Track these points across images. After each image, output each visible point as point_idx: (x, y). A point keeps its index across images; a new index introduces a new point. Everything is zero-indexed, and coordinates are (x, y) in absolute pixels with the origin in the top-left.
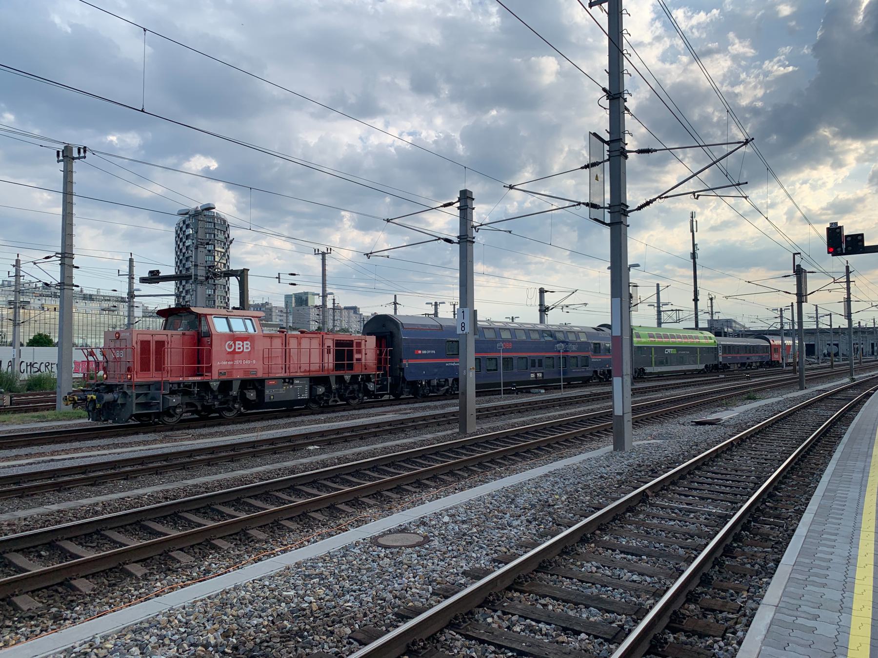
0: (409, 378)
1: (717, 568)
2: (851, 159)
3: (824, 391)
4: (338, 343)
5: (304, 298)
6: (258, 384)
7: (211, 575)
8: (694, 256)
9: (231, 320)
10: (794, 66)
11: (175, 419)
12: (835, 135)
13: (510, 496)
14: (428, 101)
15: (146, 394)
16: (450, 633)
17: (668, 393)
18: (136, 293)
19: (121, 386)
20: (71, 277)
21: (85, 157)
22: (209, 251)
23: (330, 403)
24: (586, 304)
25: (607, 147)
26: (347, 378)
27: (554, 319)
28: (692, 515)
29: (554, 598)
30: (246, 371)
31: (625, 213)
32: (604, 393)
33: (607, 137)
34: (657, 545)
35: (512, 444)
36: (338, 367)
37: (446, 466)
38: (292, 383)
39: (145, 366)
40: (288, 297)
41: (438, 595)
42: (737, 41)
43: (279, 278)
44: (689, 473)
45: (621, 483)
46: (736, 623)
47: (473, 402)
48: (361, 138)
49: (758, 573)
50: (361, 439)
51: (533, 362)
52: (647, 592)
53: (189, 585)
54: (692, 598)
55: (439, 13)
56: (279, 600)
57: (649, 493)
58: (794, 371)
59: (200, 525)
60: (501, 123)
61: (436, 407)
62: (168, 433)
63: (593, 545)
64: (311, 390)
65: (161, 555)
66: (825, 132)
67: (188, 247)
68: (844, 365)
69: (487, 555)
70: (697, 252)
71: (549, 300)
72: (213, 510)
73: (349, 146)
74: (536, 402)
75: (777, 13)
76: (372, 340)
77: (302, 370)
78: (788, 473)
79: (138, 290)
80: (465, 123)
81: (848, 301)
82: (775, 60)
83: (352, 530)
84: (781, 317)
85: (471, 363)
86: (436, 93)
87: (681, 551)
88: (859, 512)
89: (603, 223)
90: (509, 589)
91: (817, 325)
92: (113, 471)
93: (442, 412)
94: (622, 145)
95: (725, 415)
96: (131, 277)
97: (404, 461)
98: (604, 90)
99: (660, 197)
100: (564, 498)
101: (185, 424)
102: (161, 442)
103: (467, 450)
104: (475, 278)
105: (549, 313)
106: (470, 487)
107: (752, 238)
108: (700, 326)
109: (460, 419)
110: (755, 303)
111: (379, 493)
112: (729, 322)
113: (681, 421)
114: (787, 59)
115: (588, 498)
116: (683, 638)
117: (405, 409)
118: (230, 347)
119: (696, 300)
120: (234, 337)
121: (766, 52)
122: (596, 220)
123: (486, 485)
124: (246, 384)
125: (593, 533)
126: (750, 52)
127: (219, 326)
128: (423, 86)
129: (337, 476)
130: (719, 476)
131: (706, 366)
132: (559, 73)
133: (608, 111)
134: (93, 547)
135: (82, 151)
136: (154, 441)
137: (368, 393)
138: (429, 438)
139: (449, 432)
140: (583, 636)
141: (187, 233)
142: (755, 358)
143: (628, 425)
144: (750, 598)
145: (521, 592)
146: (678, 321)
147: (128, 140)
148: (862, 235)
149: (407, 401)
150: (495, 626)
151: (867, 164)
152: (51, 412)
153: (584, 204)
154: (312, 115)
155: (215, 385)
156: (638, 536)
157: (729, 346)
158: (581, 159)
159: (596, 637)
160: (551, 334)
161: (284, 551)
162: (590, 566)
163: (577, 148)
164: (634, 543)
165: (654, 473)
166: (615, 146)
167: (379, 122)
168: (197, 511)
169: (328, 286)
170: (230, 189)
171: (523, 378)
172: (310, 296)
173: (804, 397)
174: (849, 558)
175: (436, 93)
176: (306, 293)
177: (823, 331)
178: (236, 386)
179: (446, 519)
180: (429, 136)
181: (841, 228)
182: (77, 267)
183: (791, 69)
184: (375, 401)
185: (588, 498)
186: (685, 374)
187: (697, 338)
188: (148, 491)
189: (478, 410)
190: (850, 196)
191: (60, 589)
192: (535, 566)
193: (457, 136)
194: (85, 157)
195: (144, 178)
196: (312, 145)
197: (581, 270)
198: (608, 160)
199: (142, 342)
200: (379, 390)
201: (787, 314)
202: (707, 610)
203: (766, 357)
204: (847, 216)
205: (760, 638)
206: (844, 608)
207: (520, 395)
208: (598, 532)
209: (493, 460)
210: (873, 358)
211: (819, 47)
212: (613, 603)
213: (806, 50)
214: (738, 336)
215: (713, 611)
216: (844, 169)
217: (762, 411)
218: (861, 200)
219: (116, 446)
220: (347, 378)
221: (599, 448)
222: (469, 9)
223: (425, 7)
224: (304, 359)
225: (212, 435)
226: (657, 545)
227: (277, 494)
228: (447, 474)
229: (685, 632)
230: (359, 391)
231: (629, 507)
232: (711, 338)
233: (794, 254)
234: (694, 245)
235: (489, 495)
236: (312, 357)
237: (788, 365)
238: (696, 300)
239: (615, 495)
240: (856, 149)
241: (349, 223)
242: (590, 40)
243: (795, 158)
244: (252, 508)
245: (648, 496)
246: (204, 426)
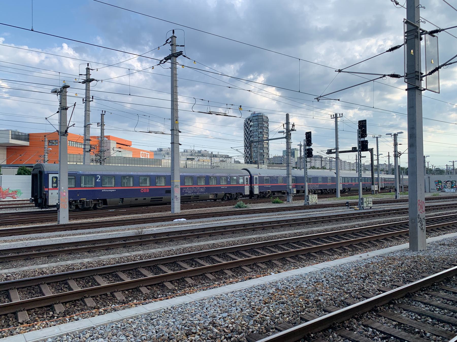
35: (384, 233)
103: (370, 232)
153: (388, 75)
168: (233, 253)
188: (304, 231)
209: (331, 249)
239: (446, 267)
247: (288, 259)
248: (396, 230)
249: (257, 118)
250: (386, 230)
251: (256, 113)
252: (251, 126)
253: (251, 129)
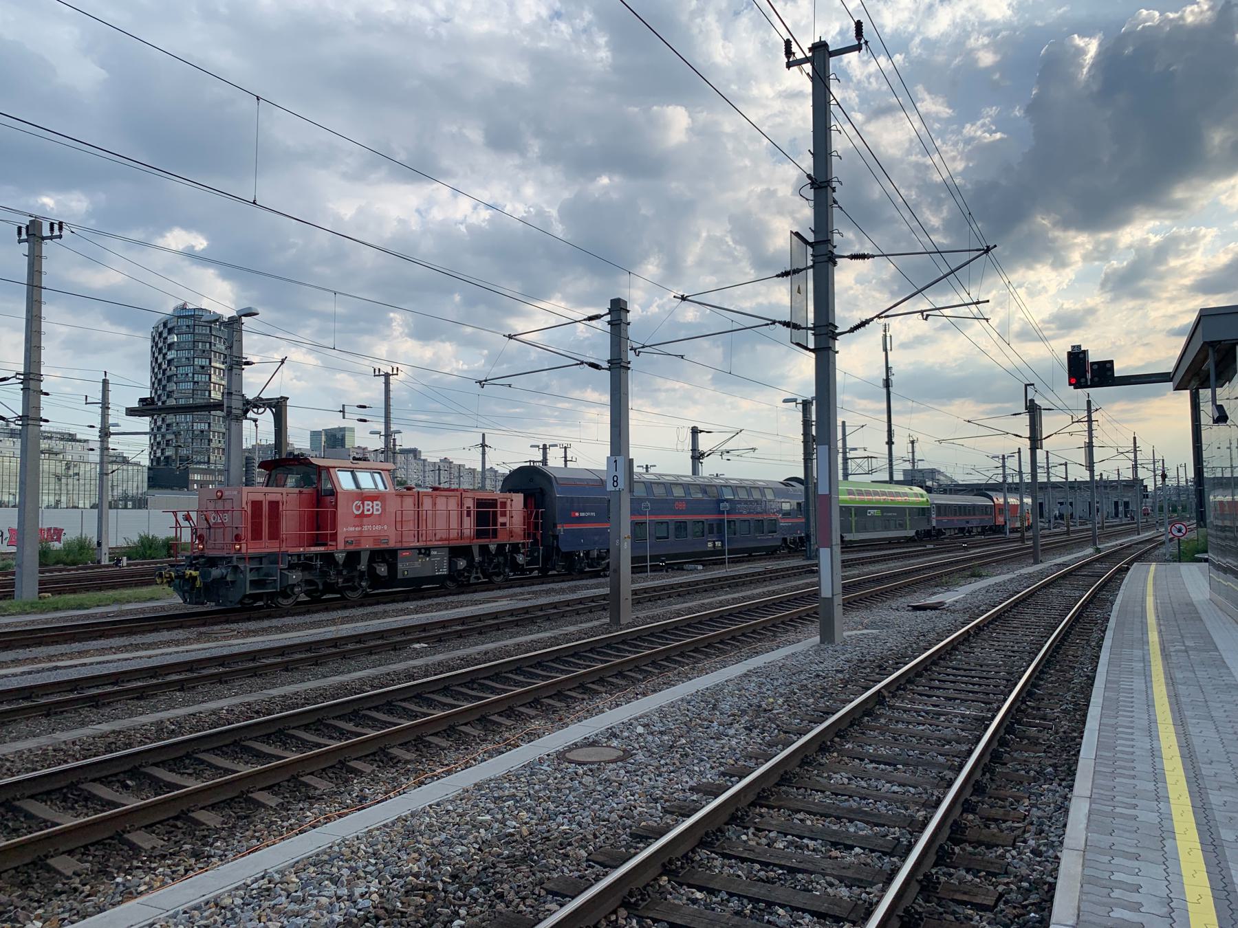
0: (564, 549)
1: (988, 775)
2: (1076, 256)
3: (1065, 565)
4: (480, 503)
5: (339, 436)
6: (388, 556)
7: (369, 802)
8: (887, 384)
9: (358, 474)
10: (1003, 132)
11: (291, 601)
12: (1055, 225)
13: (712, 699)
14: (512, 161)
15: (258, 569)
16: (704, 853)
17: (866, 569)
18: (112, 430)
19: (228, 559)
20: (38, 408)
21: (60, 237)
22: (203, 367)
23: (472, 581)
24: (754, 449)
25: (810, 250)
26: (493, 547)
27: (709, 468)
28: (942, 719)
29: (809, 813)
30: (377, 540)
31: (834, 336)
32: (782, 570)
33: (811, 238)
34: (911, 753)
36: (479, 534)
38: (429, 555)
39: (256, 535)
40: (315, 435)
41: (672, 813)
42: (927, 97)
43: (343, 412)
44: (926, 670)
45: (845, 683)
46: (1024, 832)
47: (628, 583)
48: (418, 211)
49: (1035, 780)
50: (480, 633)
51: (711, 526)
52: (916, 803)
53: (347, 814)
54: (968, 807)
55: (526, 41)
56: (474, 826)
57: (886, 694)
58: (1022, 539)
60: (615, 196)
61: (563, 591)
62: (202, 629)
63: (835, 754)
64: (452, 564)
65: (288, 781)
66: (1043, 221)
67: (170, 362)
68: (1082, 531)
69: (712, 768)
70: (892, 378)
71: (705, 443)
72: (328, 726)
73: (400, 221)
74: (697, 583)
75: (976, 61)
76: (518, 499)
77: (438, 537)
78: (1044, 666)
79: (117, 425)
80: (566, 195)
81: (1090, 446)
82: (979, 123)
83: (525, 746)
84: (1004, 466)
85: (626, 530)
86: (522, 151)
87: (941, 759)
88: (1150, 704)
89: (806, 348)
90: (754, 804)
91: (1048, 477)
92: (155, 681)
93: (575, 596)
94: (830, 248)
95: (949, 597)
96: (105, 406)
97: (552, 661)
98: (809, 176)
99: (878, 316)
100: (780, 701)
101: (301, 609)
102: (198, 640)
104: (631, 413)
105: (704, 461)
106: (654, 691)
107: (955, 360)
108: (895, 478)
109: (611, 604)
110: (968, 447)
111: (537, 701)
112: (933, 472)
113: (894, 606)
114: (993, 123)
115: (811, 700)
116: (970, 849)
117: (522, 594)
118: (358, 508)
119: (890, 443)
120: (362, 496)
121: (966, 112)
122: (798, 344)
123: (673, 688)
124: (379, 555)
125: (832, 741)
126: (945, 112)
127: (345, 481)
128: (502, 140)
129: (473, 681)
130: (962, 672)
131: (917, 533)
132: (691, 130)
133: (812, 203)
134: (190, 775)
135: (56, 227)
136: (187, 641)
137: (515, 567)
138: (573, 632)
139: (596, 623)
140: (857, 850)
141: (169, 341)
142: (975, 521)
143: (838, 610)
144: (1033, 805)
145: (769, 807)
146: (870, 472)
147: (74, 204)
148: (1111, 362)
149: (560, 578)
150: (752, 843)
151: (1097, 263)
152: (8, 602)
154: (345, 176)
155: (340, 557)
156: (885, 743)
157: (946, 506)
158: (724, 247)
159: (872, 851)
160: (704, 488)
161: (449, 773)
162: (840, 778)
163: (718, 233)
164: (882, 751)
165: (883, 671)
166: (822, 249)
167: (441, 191)
169: (393, 421)
170: (225, 276)
171: (699, 549)
172: (347, 433)
173: (1041, 574)
174: (1152, 749)
175: (522, 151)
176: (343, 429)
177: (1055, 486)
178: (365, 558)
179: (640, 730)
180: (516, 209)
181: (1085, 352)
182: (47, 394)
183: (998, 136)
184: (521, 576)
185: (811, 700)
186: (891, 543)
187: (906, 494)
188: (224, 704)
189: (635, 592)
190: (1078, 306)
191: (179, 824)
192: (776, 779)
193: (554, 212)
194: (60, 237)
195: (95, 261)
196: (347, 218)
197: (729, 399)
198: (812, 267)
199: (253, 502)
200: (528, 564)
201: (1012, 464)
202: (987, 820)
203: (987, 521)
204: (1075, 332)
205: (1083, 826)
206: (1160, 797)
207: (671, 573)
208: (837, 739)
209: (582, 686)
210: (1117, 521)
211: (1033, 108)
212: (880, 815)
213: (1018, 112)
214: (945, 492)
215: (996, 820)
216: (1068, 270)
217: (1010, 590)
218: (1091, 311)
219: (137, 647)
220: (493, 547)
221: (799, 641)
222: (568, 37)
223: (506, 32)
224: (441, 524)
225: (265, 631)
226: (911, 753)
227: (403, 704)
228: (616, 676)
229: (970, 843)
230: (505, 565)
231: (865, 710)
232: (922, 496)
233: (1026, 385)
234: (888, 369)
235: (682, 700)
236: (450, 523)
237: (1014, 530)
238: (890, 443)
240: (1083, 244)
241: (400, 330)
242: (734, 87)
243: (1007, 253)
245: (884, 697)
246: (249, 620)
247: (495, 718)
248: (630, 652)
249: (191, 323)
250: (619, 650)
251: (190, 307)
252: (170, 347)
253: (171, 355)
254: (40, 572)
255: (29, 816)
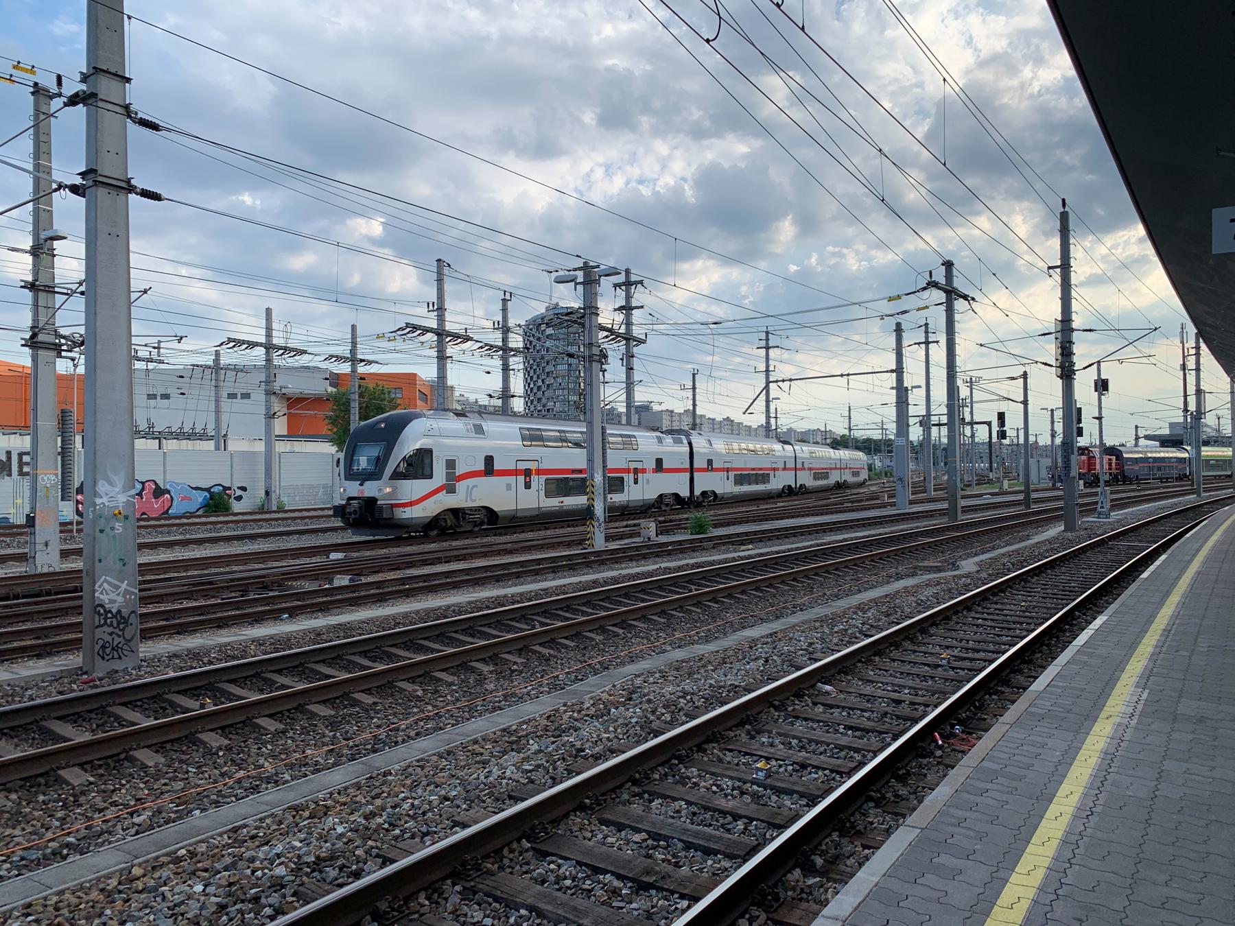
17: (828, 538)
37: (572, 625)
59: (284, 687)
129: (340, 657)
175: (634, 128)
244: (391, 657)
254: (61, 532)
255: (118, 718)
